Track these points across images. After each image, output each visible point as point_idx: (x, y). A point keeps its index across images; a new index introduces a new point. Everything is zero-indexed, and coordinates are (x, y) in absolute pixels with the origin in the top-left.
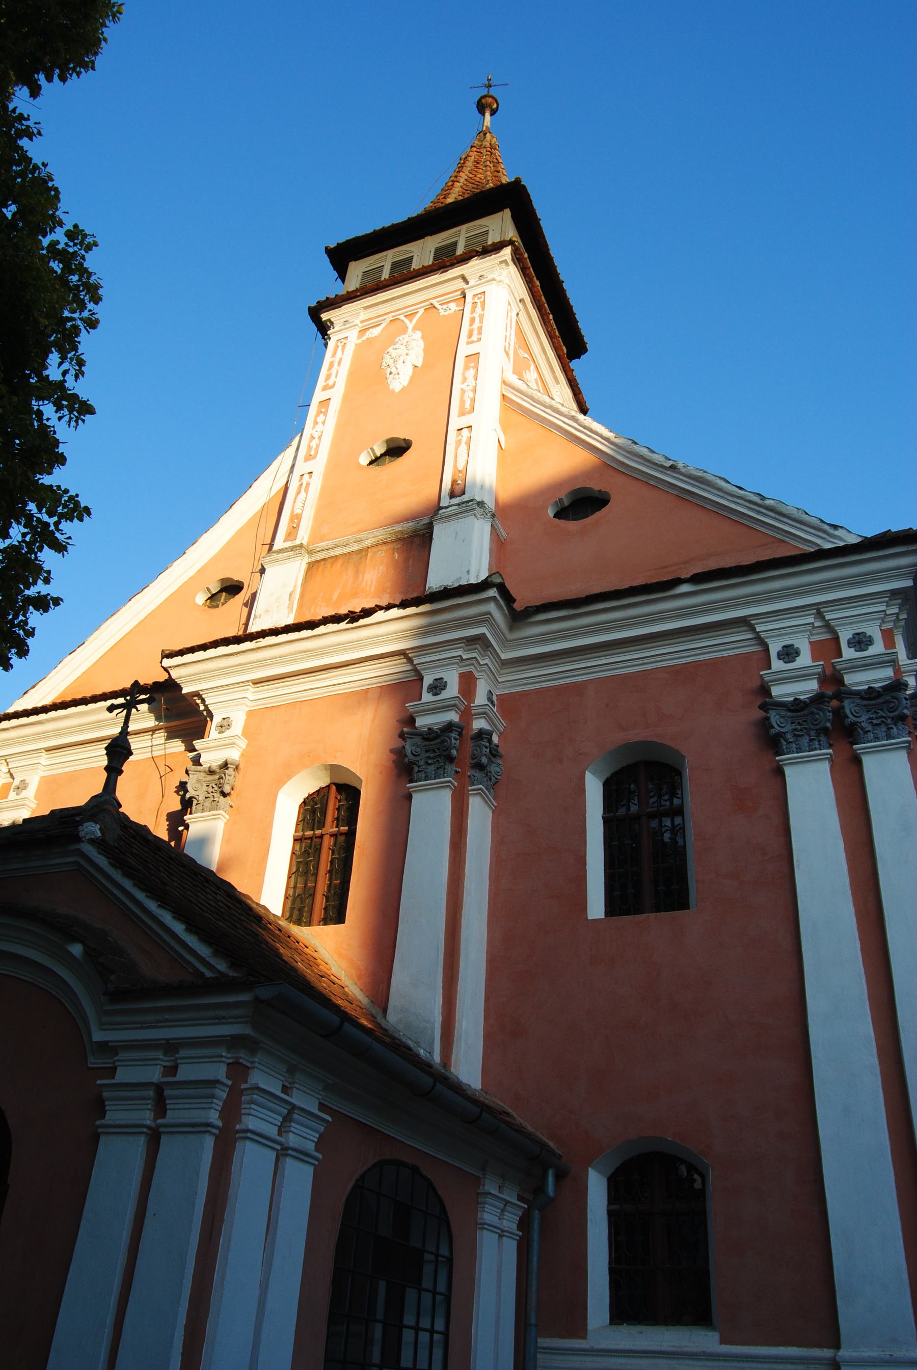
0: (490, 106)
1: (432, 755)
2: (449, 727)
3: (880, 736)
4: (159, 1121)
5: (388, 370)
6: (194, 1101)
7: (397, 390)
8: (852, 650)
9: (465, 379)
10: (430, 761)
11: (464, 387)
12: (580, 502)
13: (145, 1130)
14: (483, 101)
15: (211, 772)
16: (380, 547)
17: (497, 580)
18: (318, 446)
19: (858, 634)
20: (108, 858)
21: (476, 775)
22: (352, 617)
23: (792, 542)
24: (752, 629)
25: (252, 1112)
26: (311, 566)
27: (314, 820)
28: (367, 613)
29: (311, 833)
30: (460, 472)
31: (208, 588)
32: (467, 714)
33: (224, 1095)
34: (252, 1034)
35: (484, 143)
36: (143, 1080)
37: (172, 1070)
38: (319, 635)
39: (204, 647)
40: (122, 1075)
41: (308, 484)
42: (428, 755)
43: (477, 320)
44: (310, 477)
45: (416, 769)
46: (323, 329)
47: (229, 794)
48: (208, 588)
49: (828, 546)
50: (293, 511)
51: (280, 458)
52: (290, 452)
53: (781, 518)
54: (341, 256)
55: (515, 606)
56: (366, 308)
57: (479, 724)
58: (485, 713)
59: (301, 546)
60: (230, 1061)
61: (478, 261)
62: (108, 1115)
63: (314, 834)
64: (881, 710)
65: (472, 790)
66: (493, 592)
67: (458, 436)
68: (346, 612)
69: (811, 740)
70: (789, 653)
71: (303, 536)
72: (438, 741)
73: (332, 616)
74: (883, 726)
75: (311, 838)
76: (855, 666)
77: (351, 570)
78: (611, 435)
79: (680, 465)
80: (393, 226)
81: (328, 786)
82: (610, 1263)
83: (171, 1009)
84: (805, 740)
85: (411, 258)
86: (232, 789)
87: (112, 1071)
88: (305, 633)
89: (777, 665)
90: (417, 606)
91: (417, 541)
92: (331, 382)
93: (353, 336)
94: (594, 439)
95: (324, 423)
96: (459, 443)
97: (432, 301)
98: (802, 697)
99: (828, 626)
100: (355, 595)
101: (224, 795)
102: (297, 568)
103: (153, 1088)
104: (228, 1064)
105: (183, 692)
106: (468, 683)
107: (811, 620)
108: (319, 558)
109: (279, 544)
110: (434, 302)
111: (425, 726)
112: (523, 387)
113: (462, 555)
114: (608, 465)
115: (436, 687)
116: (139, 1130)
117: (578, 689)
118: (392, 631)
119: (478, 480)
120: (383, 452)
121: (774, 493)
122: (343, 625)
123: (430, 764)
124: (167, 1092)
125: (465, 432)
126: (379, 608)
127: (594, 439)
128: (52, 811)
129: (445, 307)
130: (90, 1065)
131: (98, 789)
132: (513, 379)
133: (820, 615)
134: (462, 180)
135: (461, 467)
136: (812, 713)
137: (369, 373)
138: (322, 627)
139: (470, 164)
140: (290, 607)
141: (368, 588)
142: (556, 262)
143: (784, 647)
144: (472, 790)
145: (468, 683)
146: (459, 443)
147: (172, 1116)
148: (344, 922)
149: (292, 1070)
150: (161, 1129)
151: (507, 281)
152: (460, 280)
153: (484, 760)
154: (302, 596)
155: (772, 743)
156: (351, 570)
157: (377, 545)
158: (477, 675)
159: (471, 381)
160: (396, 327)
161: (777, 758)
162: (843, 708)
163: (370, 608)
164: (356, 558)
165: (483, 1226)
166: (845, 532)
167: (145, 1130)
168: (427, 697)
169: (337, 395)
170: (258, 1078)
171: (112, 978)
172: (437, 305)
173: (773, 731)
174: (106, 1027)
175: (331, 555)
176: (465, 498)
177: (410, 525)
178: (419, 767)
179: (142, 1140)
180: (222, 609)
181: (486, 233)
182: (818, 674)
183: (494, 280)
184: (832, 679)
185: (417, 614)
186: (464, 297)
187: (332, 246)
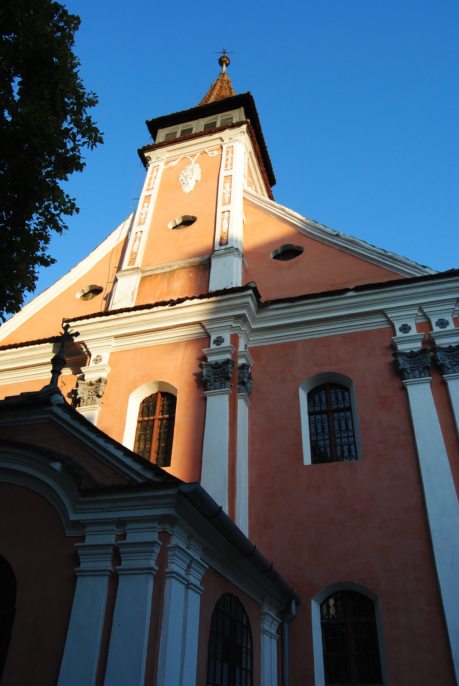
0: (226, 62)
1: (217, 377)
2: (227, 362)
3: (456, 370)
4: (118, 567)
5: (182, 182)
6: (140, 555)
7: (187, 192)
8: (438, 327)
9: (224, 188)
10: (216, 380)
11: (224, 191)
12: (288, 252)
13: (108, 573)
14: (222, 59)
15: (91, 384)
16: (181, 270)
17: (253, 285)
18: (145, 218)
19: (441, 320)
20: (70, 414)
21: (241, 388)
22: (172, 303)
23: (401, 274)
24: (386, 316)
25: (175, 561)
26: (143, 279)
27: (149, 411)
28: (180, 301)
29: (148, 418)
30: (224, 233)
31: (83, 290)
32: (235, 355)
33: (158, 551)
34: (175, 514)
35: (224, 79)
36: (105, 543)
37: (124, 536)
38: (153, 312)
39: (87, 317)
40: (89, 540)
41: (140, 237)
42: (215, 376)
43: (230, 159)
44: (142, 234)
45: (209, 384)
46: (145, 162)
47: (101, 396)
48: (83, 290)
49: (418, 275)
50: (132, 250)
51: (122, 225)
52: (128, 221)
53: (396, 262)
54: (154, 126)
55: (261, 300)
56: (168, 151)
57: (241, 361)
58: (245, 355)
59: (138, 268)
60: (161, 531)
61: (229, 131)
62: (82, 565)
63: (149, 419)
64: (456, 358)
65: (239, 396)
66: (250, 292)
67: (222, 215)
68: (169, 300)
69: (420, 373)
70: (405, 329)
71: (138, 263)
72: (221, 369)
73: (161, 302)
74: (457, 366)
75: (147, 421)
76: (441, 335)
77: (166, 281)
78: (303, 218)
79: (341, 234)
80: (182, 112)
81: (157, 394)
82: (323, 652)
83: (122, 500)
84: (417, 372)
85: (192, 129)
86: (103, 394)
87: (83, 538)
88: (145, 311)
89: (399, 334)
90: (209, 298)
91: (202, 267)
92: (151, 187)
93: (162, 165)
94: (294, 220)
95: (148, 207)
96: (223, 219)
97: (204, 149)
98: (414, 351)
99: (425, 315)
100: (168, 294)
101: (99, 396)
102: (136, 279)
103: (112, 547)
104: (159, 533)
105: (75, 341)
106: (235, 339)
107: (416, 312)
108: (147, 275)
109: (125, 266)
110: (206, 150)
111: (213, 361)
112: (255, 193)
113: (228, 273)
114: (300, 233)
115: (218, 341)
116: (104, 573)
117: (293, 345)
118: (195, 311)
119: (234, 237)
120: (180, 223)
121: (391, 249)
122: (167, 307)
123: (216, 381)
124: (121, 550)
125: (226, 214)
126: (187, 298)
127: (294, 220)
128: (22, 393)
129: (211, 152)
130: (67, 535)
131: (48, 383)
132: (249, 189)
133: (421, 310)
134: (215, 94)
135: (225, 230)
136: (420, 359)
137: (172, 184)
138: (155, 308)
139: (218, 87)
140: (132, 299)
141: (175, 291)
142: (264, 137)
143: (403, 325)
144: (239, 396)
145: (235, 339)
146: (223, 219)
147: (125, 564)
148: (169, 466)
149: (190, 537)
150: (119, 572)
151: (244, 141)
152: (219, 140)
153: (246, 380)
154: (139, 294)
155: (399, 373)
156: (166, 281)
157: (180, 269)
158: (239, 336)
159: (228, 189)
160: (185, 161)
161: (403, 381)
162: (436, 356)
163: (183, 298)
164: (168, 275)
165: (265, 632)
166: (429, 269)
167: (108, 573)
168: (213, 346)
169: (155, 193)
170: (175, 541)
171: (83, 481)
172: (207, 151)
173: (400, 367)
174: (78, 512)
175: (154, 273)
176: (228, 246)
177: (198, 259)
178: (210, 383)
179: (106, 579)
180: (89, 302)
181: (232, 118)
182: (422, 339)
183: (237, 140)
184: (429, 342)
185: (208, 302)
186: (222, 148)
187: (150, 120)
